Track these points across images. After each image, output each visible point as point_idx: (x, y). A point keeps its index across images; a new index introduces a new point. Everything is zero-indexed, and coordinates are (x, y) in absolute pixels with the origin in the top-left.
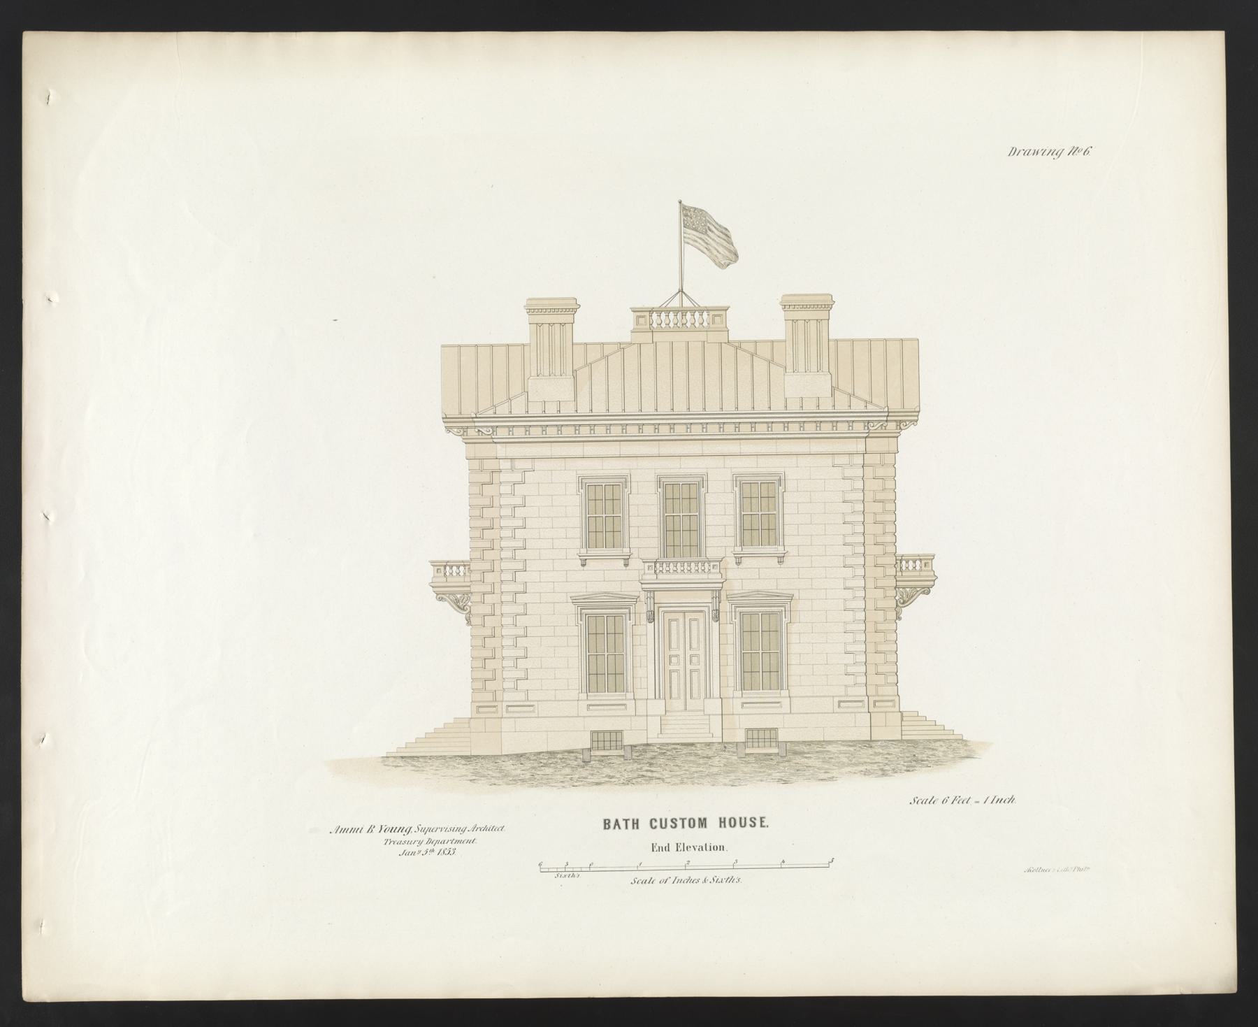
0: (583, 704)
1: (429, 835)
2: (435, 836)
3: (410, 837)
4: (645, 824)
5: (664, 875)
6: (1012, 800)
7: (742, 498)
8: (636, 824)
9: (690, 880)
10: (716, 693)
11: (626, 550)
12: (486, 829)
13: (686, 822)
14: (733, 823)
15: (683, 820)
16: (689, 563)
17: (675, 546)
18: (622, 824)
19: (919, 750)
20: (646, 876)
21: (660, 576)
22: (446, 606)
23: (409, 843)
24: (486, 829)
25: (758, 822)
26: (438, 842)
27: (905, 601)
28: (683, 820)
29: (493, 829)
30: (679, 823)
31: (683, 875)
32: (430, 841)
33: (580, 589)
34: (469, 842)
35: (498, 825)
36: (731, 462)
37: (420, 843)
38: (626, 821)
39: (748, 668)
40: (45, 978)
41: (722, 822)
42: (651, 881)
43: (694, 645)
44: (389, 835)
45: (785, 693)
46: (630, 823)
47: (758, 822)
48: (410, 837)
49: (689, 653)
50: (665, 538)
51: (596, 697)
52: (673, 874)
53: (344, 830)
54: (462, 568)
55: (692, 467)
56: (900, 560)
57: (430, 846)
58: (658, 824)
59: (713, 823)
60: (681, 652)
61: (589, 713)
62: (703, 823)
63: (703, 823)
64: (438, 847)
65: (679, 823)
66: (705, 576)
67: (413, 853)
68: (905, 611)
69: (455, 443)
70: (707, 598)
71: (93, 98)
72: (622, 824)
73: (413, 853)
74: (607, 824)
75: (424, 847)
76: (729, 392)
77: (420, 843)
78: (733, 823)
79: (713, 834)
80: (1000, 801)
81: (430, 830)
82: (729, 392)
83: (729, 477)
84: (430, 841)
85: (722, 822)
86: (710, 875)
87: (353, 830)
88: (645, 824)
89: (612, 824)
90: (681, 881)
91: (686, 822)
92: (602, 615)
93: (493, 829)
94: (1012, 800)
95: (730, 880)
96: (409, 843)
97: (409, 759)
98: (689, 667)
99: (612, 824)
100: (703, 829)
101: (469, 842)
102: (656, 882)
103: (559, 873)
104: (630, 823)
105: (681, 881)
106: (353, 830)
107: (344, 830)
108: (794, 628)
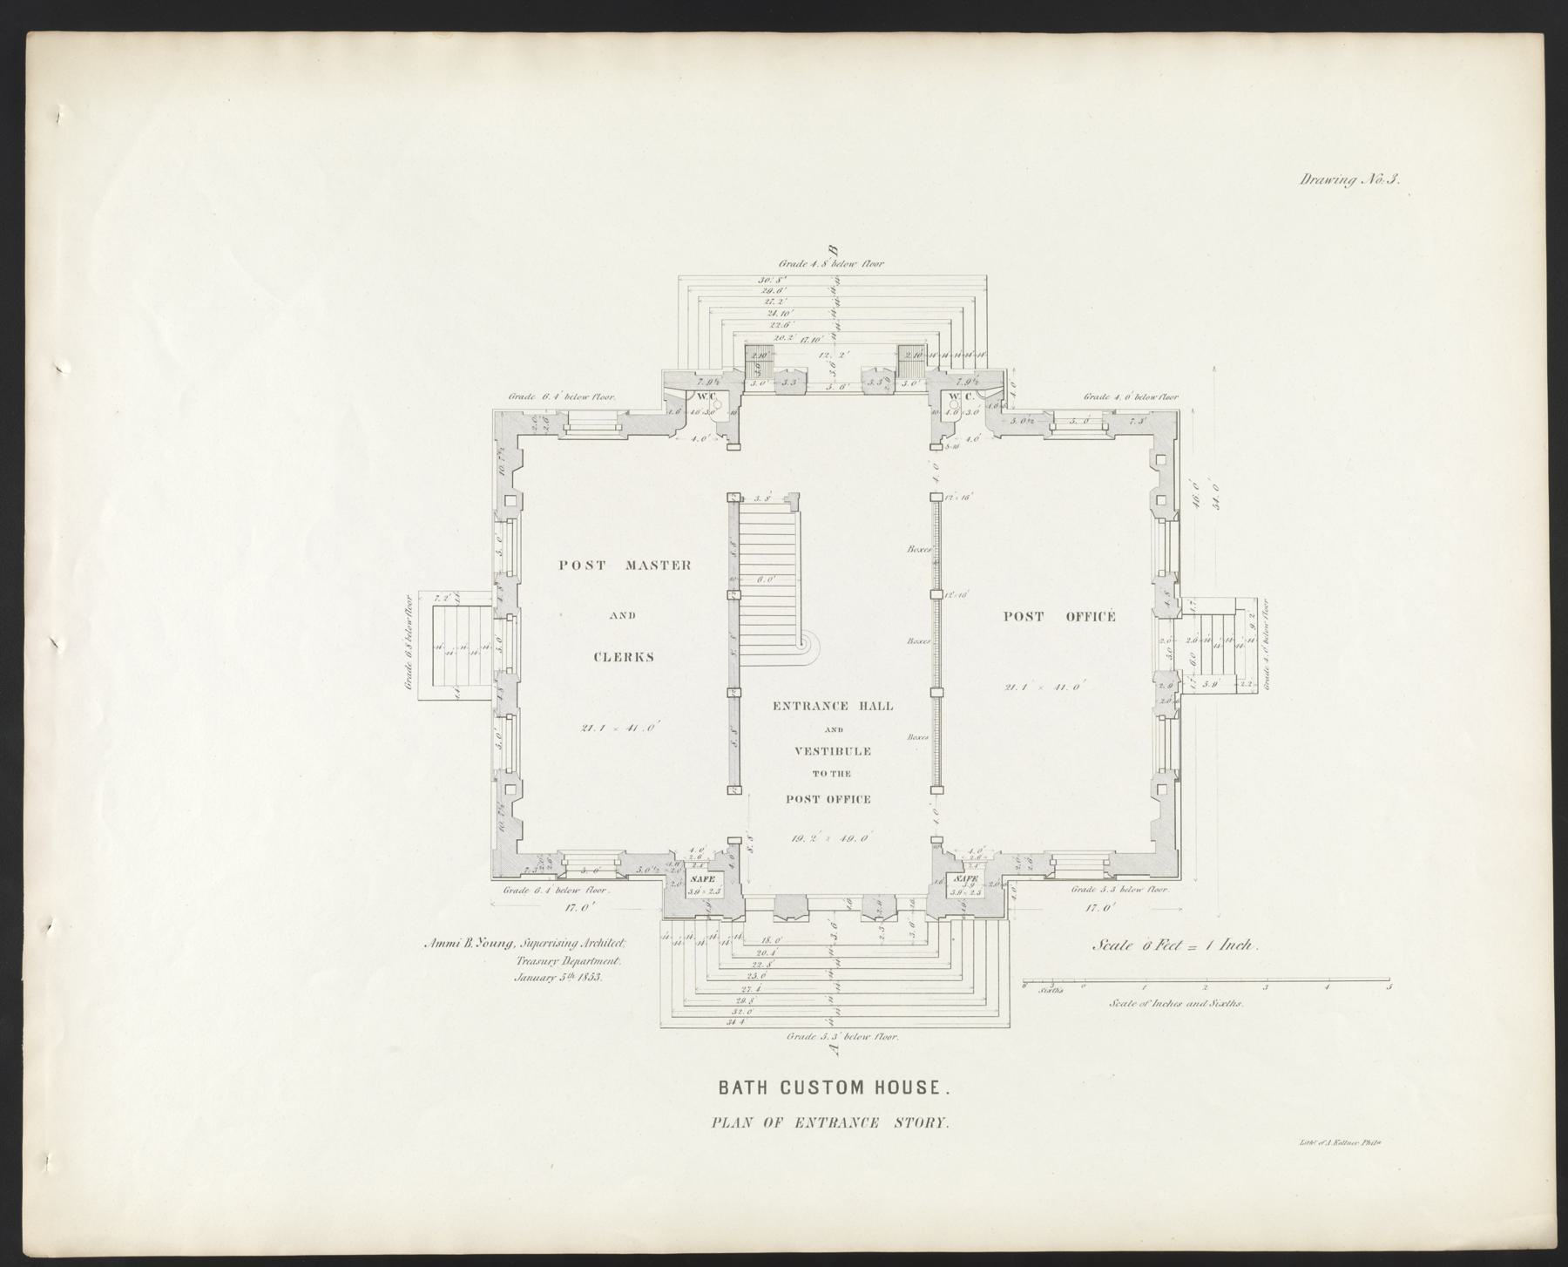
2: (577, 954)
4: (869, 1087)
6: (1247, 945)
8: (763, 1087)
13: (833, 1086)
25: (928, 1087)
30: (822, 1087)
32: (568, 960)
35: (617, 939)
40: (71, 76)
41: (879, 1087)
42: (1131, 1004)
46: (754, 1086)
47: (928, 1087)
53: (441, 944)
57: (568, 969)
58: (792, 1087)
62: (858, 1086)
64: (579, 970)
65: (822, 1087)
71: (113, 117)
72: (744, 1086)
74: (723, 1087)
76: (755, 560)
82: (755, 560)
84: (568, 960)
85: (879, 1087)
86: (808, 269)
87: (451, 944)
88: (773, 1087)
89: (731, 1087)
91: (833, 1086)
99: (731, 1087)
100: (857, 1095)
102: (758, 1123)
104: (754, 1086)
106: (451, 944)
107: (441, 944)
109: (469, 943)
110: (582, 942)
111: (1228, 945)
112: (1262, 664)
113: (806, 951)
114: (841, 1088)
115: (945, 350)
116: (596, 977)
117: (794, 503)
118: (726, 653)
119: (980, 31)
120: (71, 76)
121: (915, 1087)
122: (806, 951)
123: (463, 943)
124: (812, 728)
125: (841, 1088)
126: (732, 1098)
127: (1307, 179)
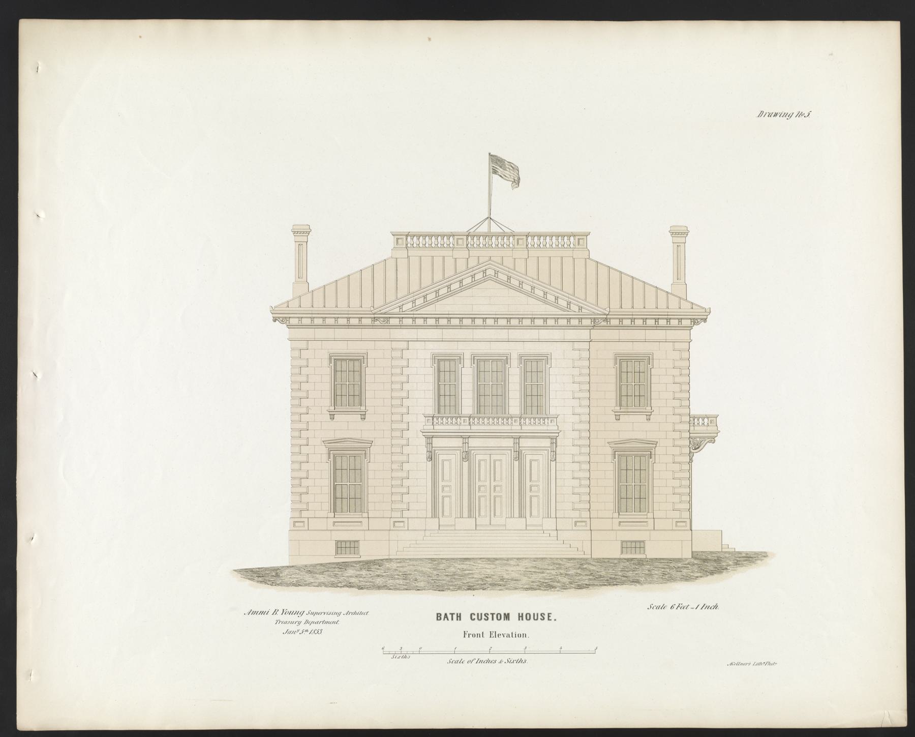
0: (616, 521)
5: (471, 657)
6: (716, 607)
7: (526, 372)
8: (459, 617)
9: (488, 661)
10: (553, 515)
11: (363, 408)
12: (355, 613)
13: (495, 616)
14: (528, 617)
15: (493, 614)
16: (535, 419)
18: (450, 617)
21: (436, 427)
25: (546, 617)
26: (313, 622)
27: (697, 447)
28: (493, 614)
29: (361, 613)
30: (490, 617)
31: (484, 658)
32: (307, 622)
33: (330, 436)
34: (334, 622)
36: (430, 345)
37: (299, 623)
38: (452, 614)
39: (624, 495)
40: (44, 45)
41: (520, 617)
42: (462, 662)
43: (482, 478)
45: (365, 515)
46: (455, 616)
47: (546, 617)
49: (493, 484)
50: (525, 402)
51: (625, 517)
52: (477, 657)
54: (706, 420)
55: (355, 348)
56: (693, 419)
59: (514, 617)
60: (487, 483)
61: (620, 528)
62: (507, 617)
63: (507, 617)
64: (310, 628)
65: (490, 617)
66: (509, 427)
67: (294, 632)
68: (697, 456)
69: (281, 328)
70: (546, 443)
72: (450, 617)
73: (294, 632)
74: (439, 616)
78: (528, 617)
79: (514, 625)
81: (317, 613)
83: (429, 356)
84: (307, 622)
85: (520, 617)
86: (505, 658)
87: (262, 613)
89: (443, 617)
90: (481, 662)
91: (495, 616)
92: (631, 455)
93: (361, 613)
94: (716, 607)
95: (521, 661)
97: (750, 558)
98: (493, 494)
99: (443, 617)
102: (465, 662)
103: (394, 655)
104: (455, 616)
105: (481, 662)
106: (262, 613)
108: (371, 466)
109: (275, 612)
110: (306, 612)
111: (705, 607)
112: (466, 658)
114: (499, 617)
116: (319, 632)
118: (647, 548)
119: (15, 480)
120: (25, 720)
124: (442, 409)
125: (499, 617)
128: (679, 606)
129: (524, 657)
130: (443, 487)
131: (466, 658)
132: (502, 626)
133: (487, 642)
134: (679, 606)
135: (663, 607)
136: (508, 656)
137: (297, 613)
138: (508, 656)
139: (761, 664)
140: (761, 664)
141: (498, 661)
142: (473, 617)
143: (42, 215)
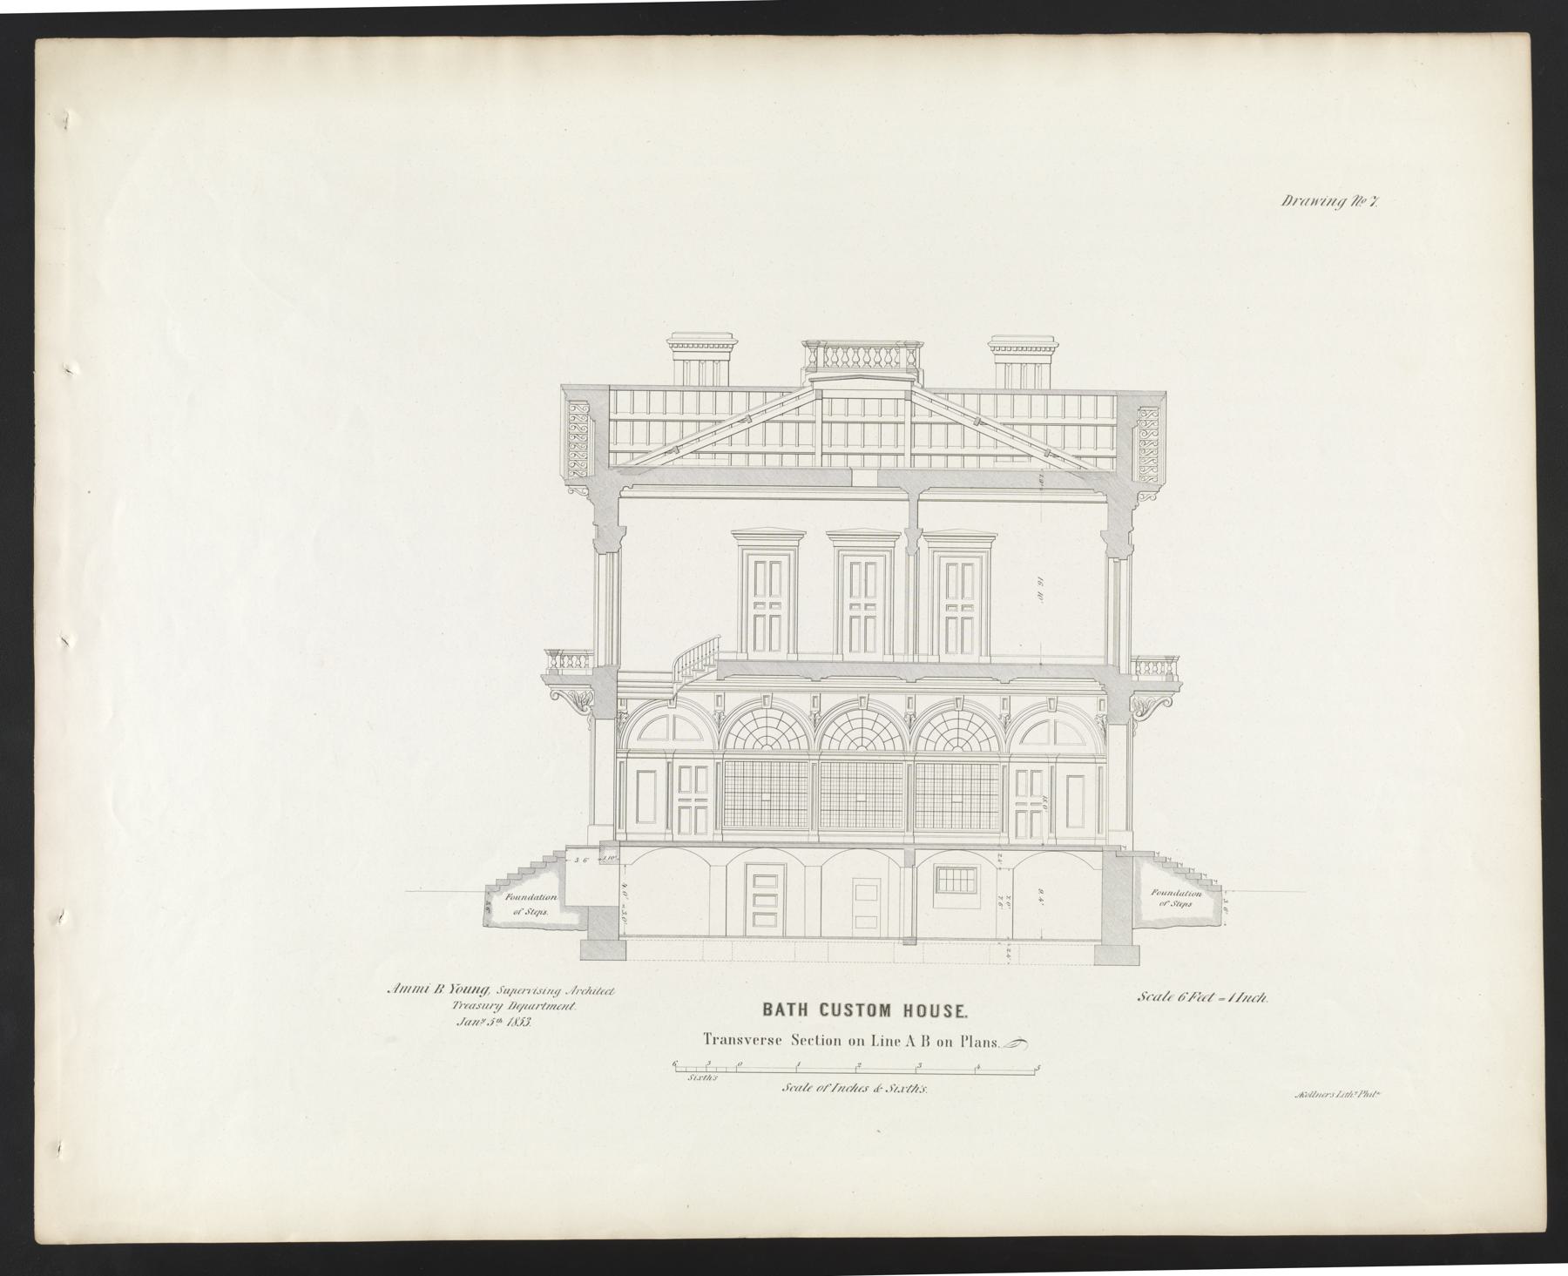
1: (515, 998)
2: (489, 1014)
3: (485, 1000)
6: (1262, 998)
8: (803, 1010)
9: (854, 1089)
13: (864, 1009)
15: (860, 1005)
17: (832, 717)
18: (786, 1009)
19: (807, 344)
20: (799, 1080)
22: (564, 707)
23: (486, 1007)
24: (589, 991)
26: (525, 1007)
28: (860, 1005)
29: (600, 992)
30: (855, 1010)
31: (848, 1081)
32: (514, 1006)
34: (565, 1007)
37: (499, 1007)
38: (791, 1005)
41: (908, 1010)
42: (807, 1088)
44: (461, 997)
46: (796, 1009)
47: (953, 1011)
48: (485, 1000)
52: (834, 1080)
53: (406, 989)
57: (515, 1013)
59: (897, 1010)
62: (886, 1010)
63: (886, 1010)
65: (855, 1010)
67: (476, 1023)
72: (786, 1009)
73: (476, 1023)
74: (767, 1009)
75: (506, 1014)
77: (499, 1007)
80: (1247, 999)
81: (515, 991)
84: (514, 1006)
85: (908, 1010)
86: (887, 1082)
87: (418, 990)
89: (774, 1010)
91: (864, 1009)
93: (600, 992)
94: (1262, 998)
96: (486, 1007)
99: (774, 1010)
101: (565, 1007)
102: (813, 1090)
104: (796, 1009)
106: (418, 990)
107: (406, 989)
109: (439, 989)
113: (602, 633)
115: (879, 815)
116: (526, 1022)
117: (553, 653)
121: (843, 1010)
122: (602, 633)
123: (433, 988)
126: (774, 1019)
127: (1289, 200)
128: (1196, 996)
129: (920, 1081)
130: (756, 604)
131: (816, 1081)
132: (879, 1025)
133: (846, 1056)
134: (1196, 996)
135: (1167, 997)
136: (892, 1080)
137: (476, 990)
138: (892, 1080)
139: (1349, 1095)
140: (1349, 1095)
141: (873, 1087)
142: (826, 1009)
143: (75, 369)
